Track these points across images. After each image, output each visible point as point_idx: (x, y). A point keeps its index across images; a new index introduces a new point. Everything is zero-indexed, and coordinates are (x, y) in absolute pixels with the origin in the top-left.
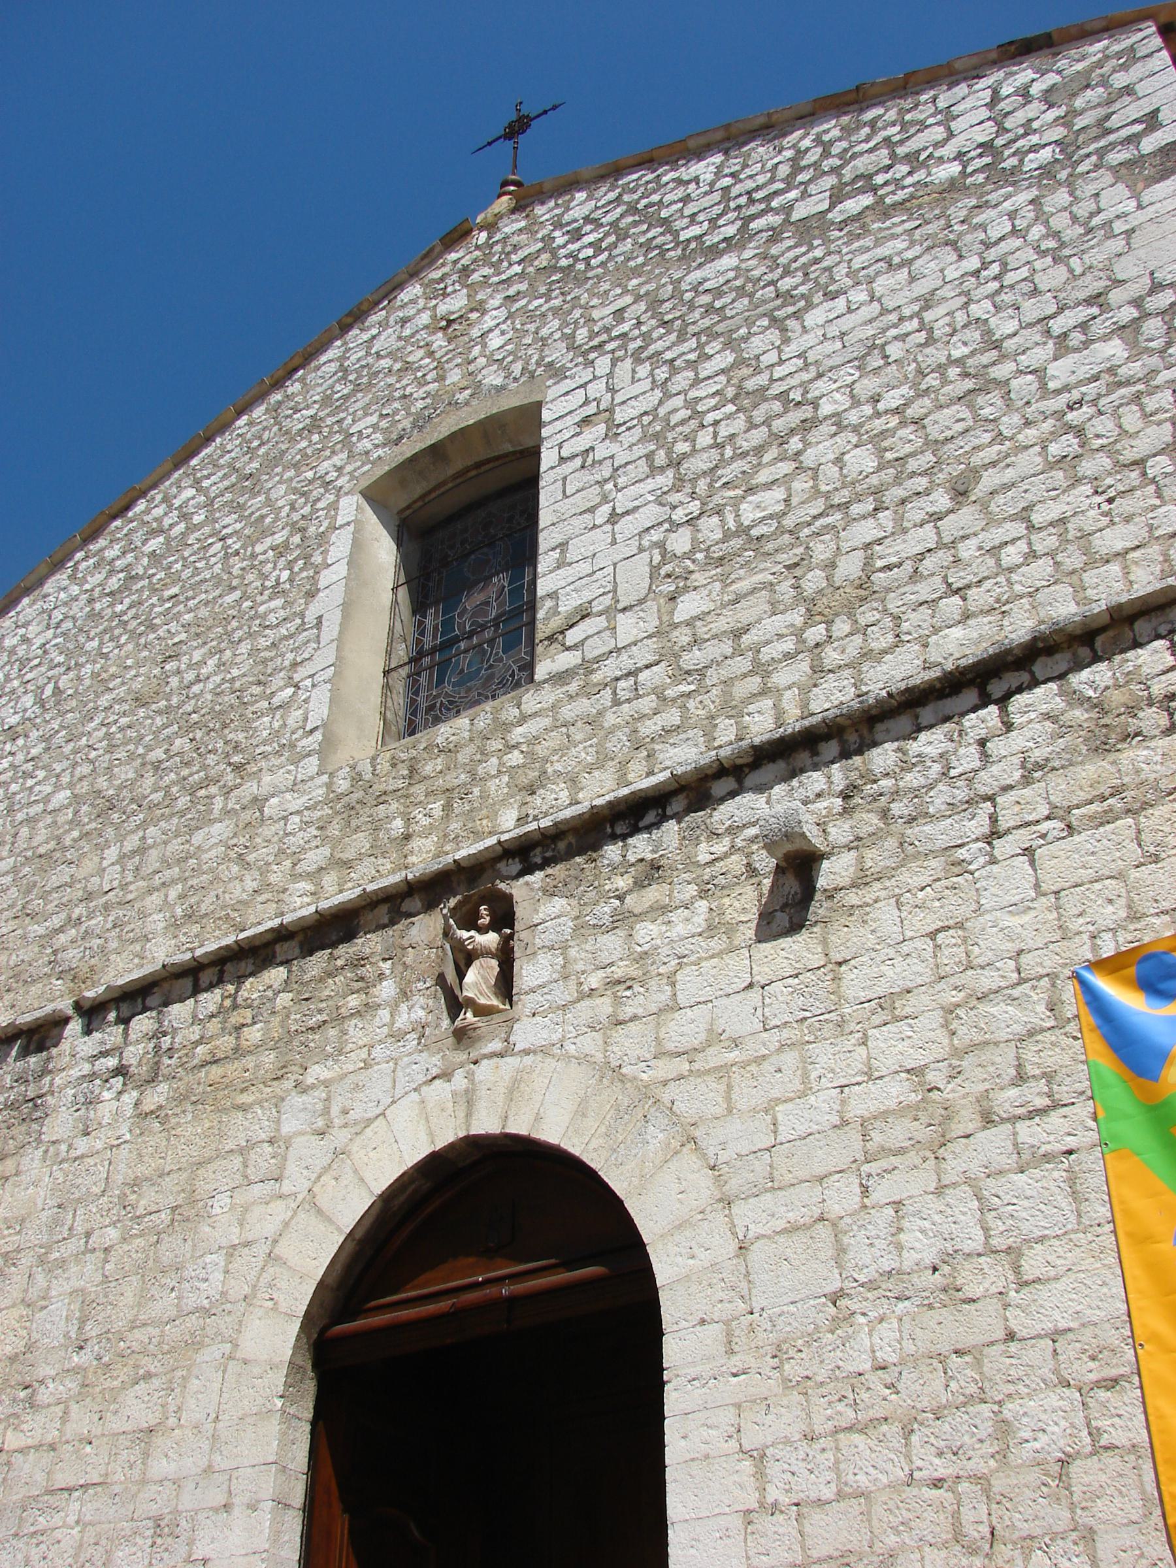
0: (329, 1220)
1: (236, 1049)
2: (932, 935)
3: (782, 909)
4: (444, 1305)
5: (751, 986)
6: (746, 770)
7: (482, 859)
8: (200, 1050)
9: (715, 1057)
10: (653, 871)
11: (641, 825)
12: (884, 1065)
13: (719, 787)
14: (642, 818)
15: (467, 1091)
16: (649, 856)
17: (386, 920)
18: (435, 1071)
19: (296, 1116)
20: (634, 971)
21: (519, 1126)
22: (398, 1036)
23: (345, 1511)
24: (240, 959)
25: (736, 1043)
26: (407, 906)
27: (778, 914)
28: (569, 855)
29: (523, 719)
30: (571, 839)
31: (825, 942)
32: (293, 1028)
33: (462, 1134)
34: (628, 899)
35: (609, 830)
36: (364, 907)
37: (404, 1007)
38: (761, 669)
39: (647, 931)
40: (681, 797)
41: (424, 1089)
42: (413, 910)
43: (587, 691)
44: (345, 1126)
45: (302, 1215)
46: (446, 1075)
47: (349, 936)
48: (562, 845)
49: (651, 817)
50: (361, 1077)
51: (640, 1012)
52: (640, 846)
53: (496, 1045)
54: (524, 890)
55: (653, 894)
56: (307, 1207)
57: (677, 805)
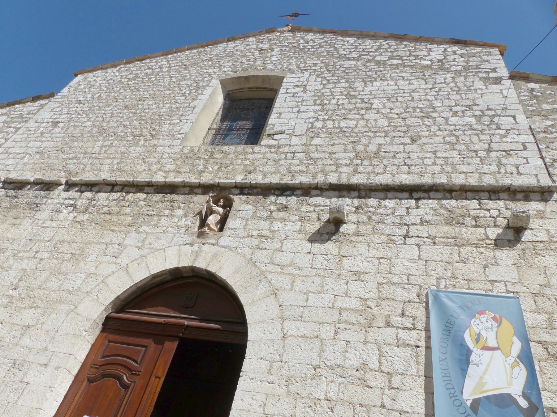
2: (379, 259)
3: (327, 233)
5: (309, 253)
7: (227, 186)
9: (291, 270)
10: (284, 208)
12: (353, 293)
14: (286, 192)
15: (197, 252)
16: (284, 203)
17: (187, 192)
18: (188, 242)
19: (132, 239)
20: (269, 235)
21: (212, 269)
22: (179, 227)
25: (300, 269)
26: (196, 190)
27: (325, 235)
28: (256, 194)
29: (253, 153)
30: (259, 190)
31: (339, 248)
32: (142, 213)
33: (190, 265)
35: (273, 192)
36: (181, 186)
37: (184, 219)
38: (337, 166)
39: (277, 225)
40: (300, 190)
41: (182, 246)
43: (276, 152)
44: (149, 248)
45: (121, 271)
46: (191, 244)
48: (255, 191)
50: (161, 235)
51: (268, 248)
52: (282, 200)
53: (213, 241)
54: (238, 200)
55: (282, 214)
56: (124, 269)
57: (298, 192)
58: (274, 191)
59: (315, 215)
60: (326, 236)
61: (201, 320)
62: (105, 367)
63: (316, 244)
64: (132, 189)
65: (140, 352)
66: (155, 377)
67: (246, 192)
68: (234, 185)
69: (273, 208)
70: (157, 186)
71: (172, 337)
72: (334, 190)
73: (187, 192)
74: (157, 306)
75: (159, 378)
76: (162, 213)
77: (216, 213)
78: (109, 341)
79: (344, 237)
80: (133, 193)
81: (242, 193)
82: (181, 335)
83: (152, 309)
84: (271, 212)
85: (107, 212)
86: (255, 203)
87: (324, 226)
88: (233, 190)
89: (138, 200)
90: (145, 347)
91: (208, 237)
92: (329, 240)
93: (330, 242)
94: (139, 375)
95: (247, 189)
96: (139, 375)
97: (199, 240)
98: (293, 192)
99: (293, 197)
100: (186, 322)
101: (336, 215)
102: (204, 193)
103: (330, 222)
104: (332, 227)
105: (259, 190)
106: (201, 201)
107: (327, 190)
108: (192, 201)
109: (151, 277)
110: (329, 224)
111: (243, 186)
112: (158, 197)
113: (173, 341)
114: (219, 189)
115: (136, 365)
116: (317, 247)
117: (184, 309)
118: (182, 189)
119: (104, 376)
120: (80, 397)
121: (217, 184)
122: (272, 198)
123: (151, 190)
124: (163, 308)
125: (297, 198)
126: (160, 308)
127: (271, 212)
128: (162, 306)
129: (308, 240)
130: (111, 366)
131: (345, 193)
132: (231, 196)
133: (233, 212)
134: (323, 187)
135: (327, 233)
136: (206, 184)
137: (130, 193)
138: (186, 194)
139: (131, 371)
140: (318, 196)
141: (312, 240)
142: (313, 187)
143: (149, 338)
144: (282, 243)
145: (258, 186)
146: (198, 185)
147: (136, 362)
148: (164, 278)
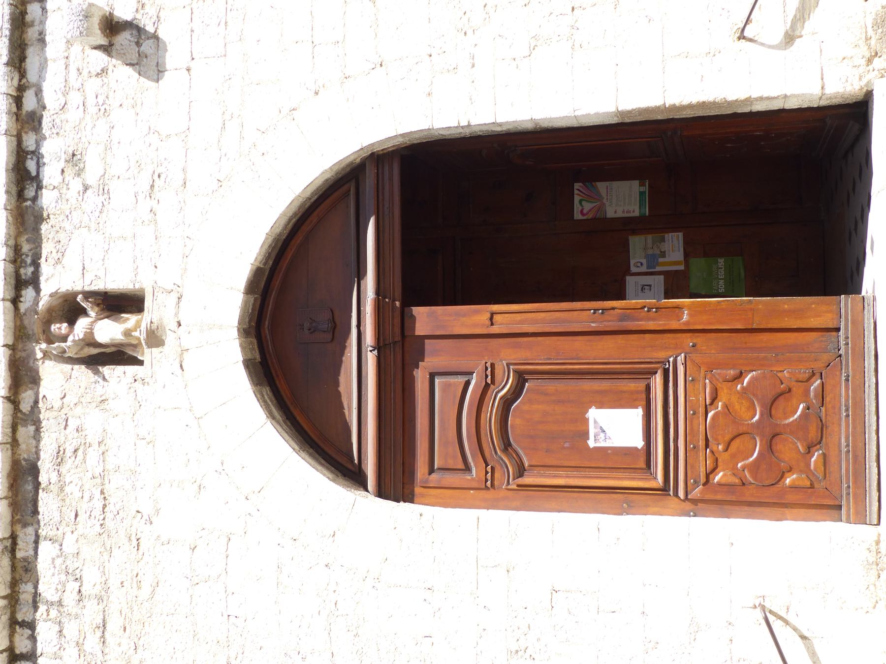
0: (104, 620)
1: (100, 599)
3: (138, 44)
4: (371, 359)
6: (24, 81)
7: (11, 324)
8: (87, 647)
11: (34, 174)
13: (29, 103)
14: (28, 172)
17: (32, 428)
23: (588, 419)
24: (17, 601)
26: (25, 407)
27: (142, 49)
28: (37, 241)
30: (23, 240)
34: (89, 182)
35: (29, 203)
36: (13, 454)
40: (25, 137)
42: (32, 401)
47: (34, 470)
48: (26, 248)
49: (31, 165)
52: (50, 174)
54: (57, 279)
57: (29, 141)
58: (26, 200)
59: (93, 85)
60: (147, 46)
61: (360, 273)
62: (487, 455)
63: (167, 61)
64: (22, 597)
65: (446, 387)
66: (492, 324)
67: (31, 269)
68: (9, 304)
69: (76, 185)
70: (13, 523)
71: (406, 321)
72: (22, 58)
73: (32, 428)
74: (339, 395)
75: (492, 314)
76: (98, 470)
77: (91, 329)
78: (431, 470)
79: (147, 7)
80: (36, 587)
81: (35, 281)
82: (398, 304)
83: (346, 406)
84: (86, 188)
85: (99, 633)
86: (62, 236)
87: (121, 56)
88: (23, 307)
89: (59, 561)
90: (432, 376)
91: (161, 319)
92: (155, 37)
93: (161, 34)
94: (492, 365)
95: (22, 271)
96: (492, 365)
97: (170, 339)
98: (27, 153)
99: (43, 150)
100: (369, 338)
101: (96, 21)
102: (35, 380)
103: (111, 45)
104: (124, 38)
105: (23, 240)
106: (56, 379)
107: (22, 74)
108: (57, 404)
109: (273, 422)
110: (117, 46)
111: (13, 282)
112: (47, 504)
113: (413, 318)
114: (20, 346)
115: (473, 382)
116: (173, 58)
117: (337, 332)
118: (23, 446)
119: (507, 446)
120: (555, 476)
121: (8, 352)
122: (47, 199)
123: (25, 536)
124: (342, 379)
125: (45, 138)
126: (342, 389)
127: (86, 188)
128: (337, 384)
129: (157, 81)
130: (484, 445)
131: (31, 34)
132: (41, 304)
133: (87, 282)
134: (16, 82)
135: (138, 44)
136: (9, 382)
137: (36, 595)
138: (38, 430)
139: (487, 386)
140: (39, 92)
141: (158, 72)
142: (14, 109)
143: (413, 379)
144: (168, 136)
145: (12, 242)
146: (10, 406)
147: (468, 383)
148: (271, 401)
